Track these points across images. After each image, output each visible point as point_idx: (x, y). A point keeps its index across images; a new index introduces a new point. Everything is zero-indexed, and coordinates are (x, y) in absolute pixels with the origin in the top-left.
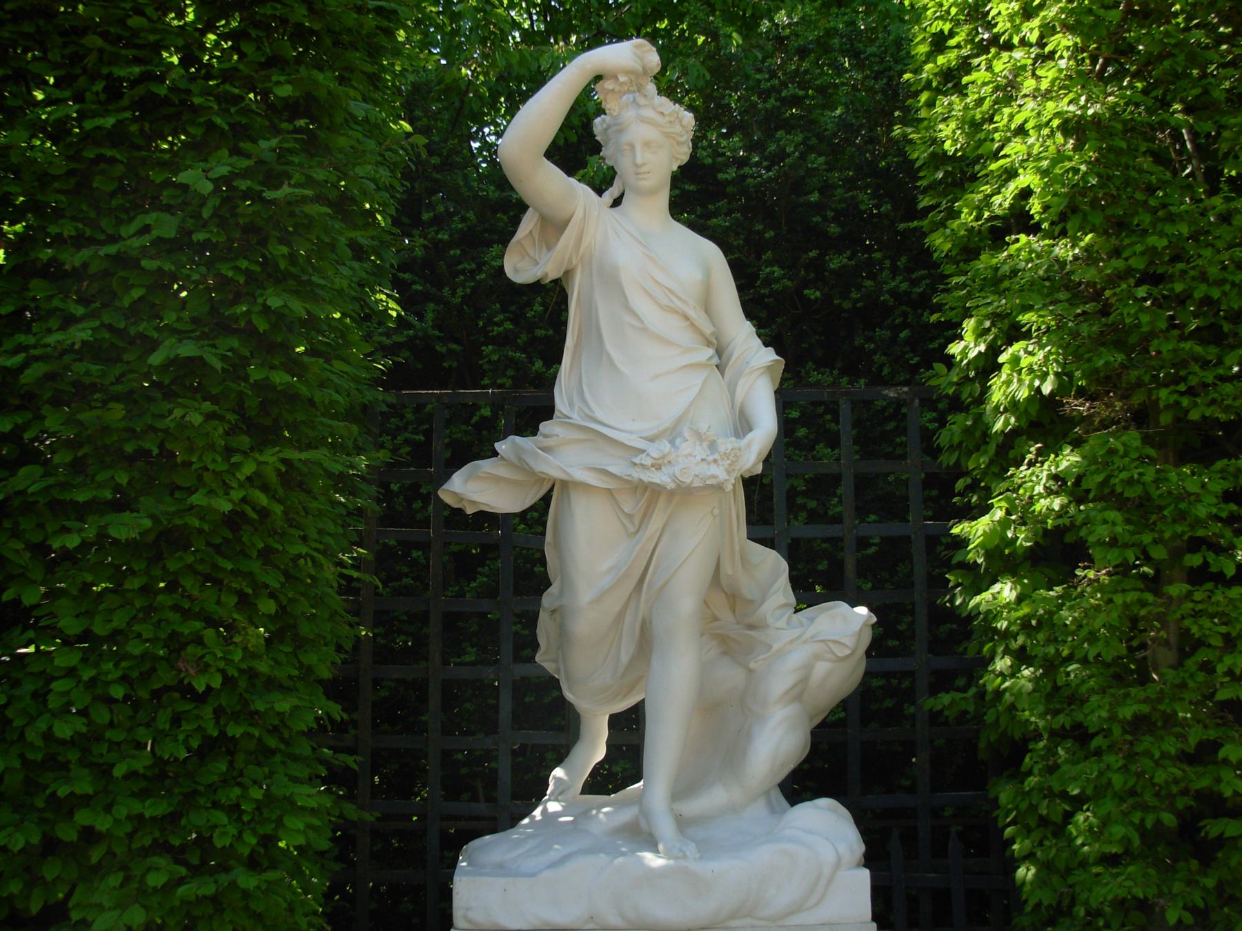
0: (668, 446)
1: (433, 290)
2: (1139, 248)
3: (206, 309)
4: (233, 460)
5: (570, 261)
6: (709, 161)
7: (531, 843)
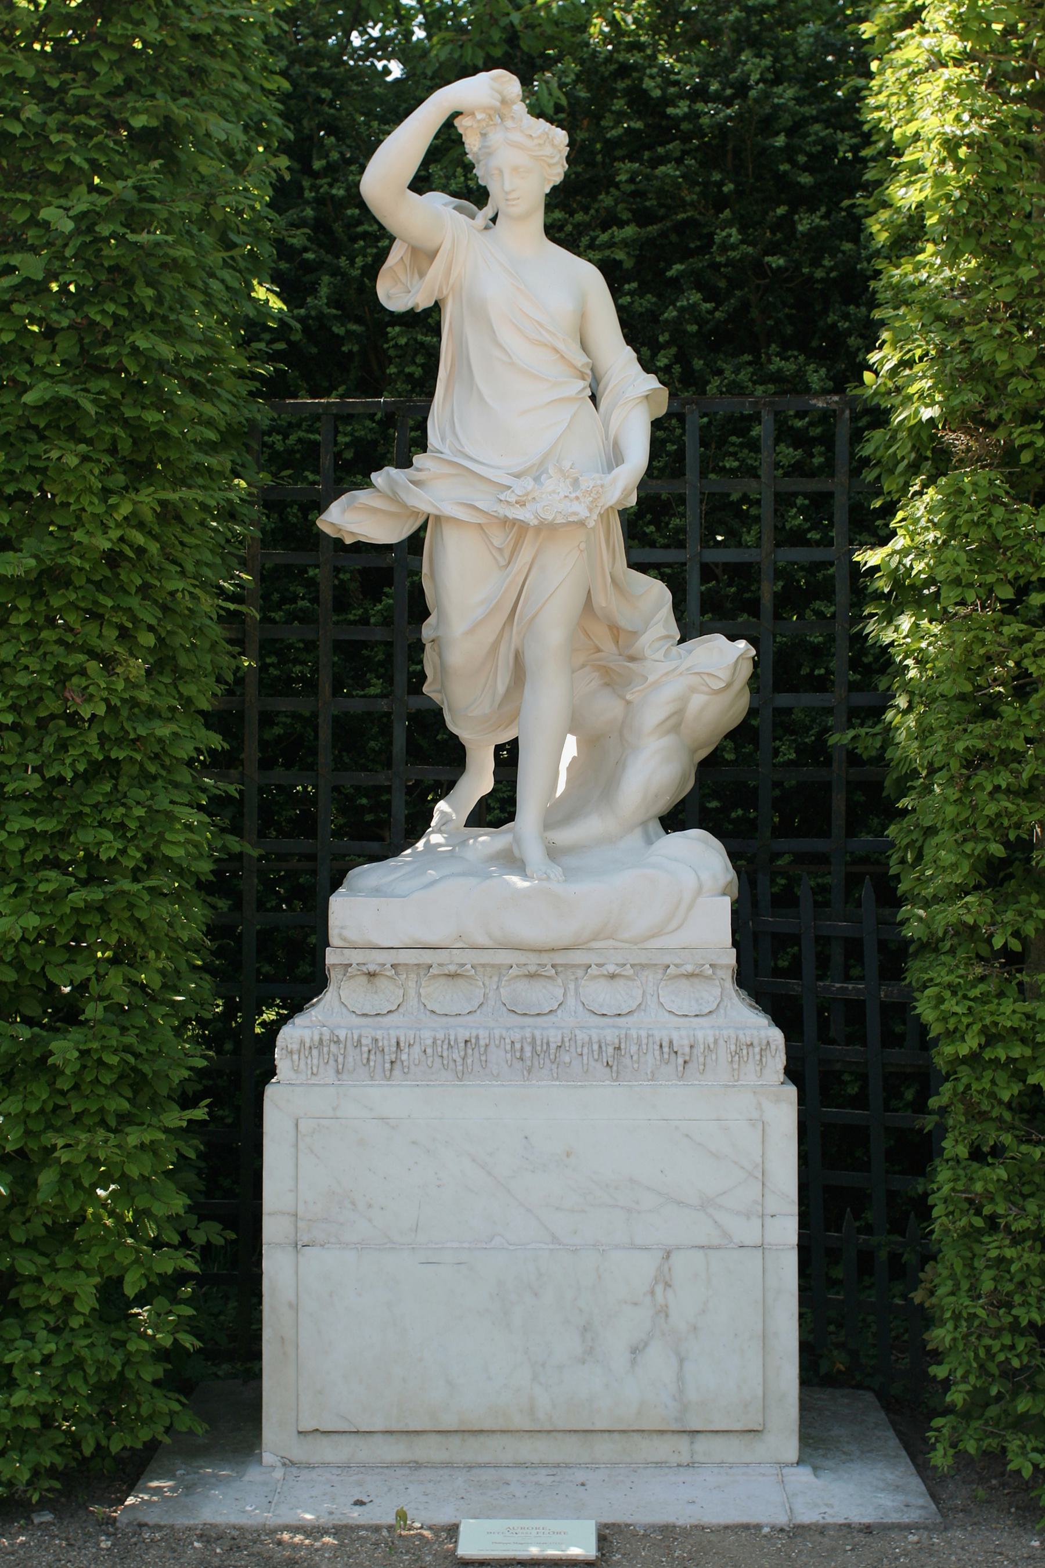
0: (532, 483)
1: (328, 258)
2: (1007, 279)
3: (77, 350)
4: (110, 502)
5: (440, 290)
6: (657, 93)
7: (407, 869)
